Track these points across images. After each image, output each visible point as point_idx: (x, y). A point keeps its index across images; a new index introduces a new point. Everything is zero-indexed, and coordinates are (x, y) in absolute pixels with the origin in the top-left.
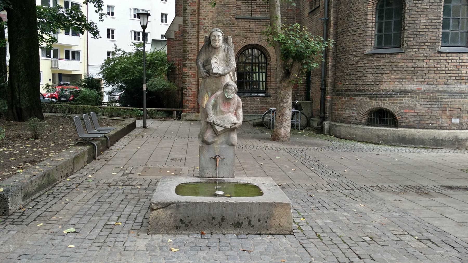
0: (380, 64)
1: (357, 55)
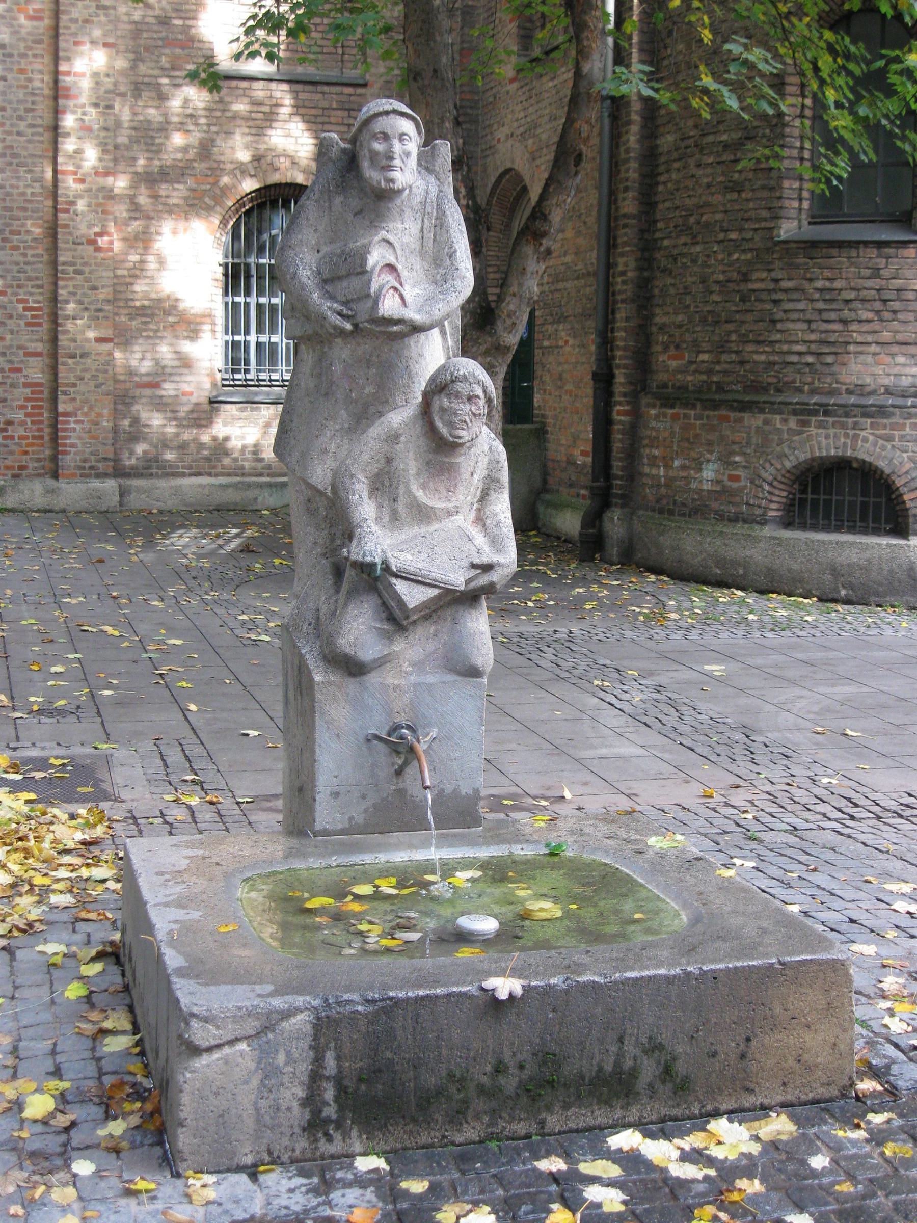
0: (838, 284)
1: (747, 246)
